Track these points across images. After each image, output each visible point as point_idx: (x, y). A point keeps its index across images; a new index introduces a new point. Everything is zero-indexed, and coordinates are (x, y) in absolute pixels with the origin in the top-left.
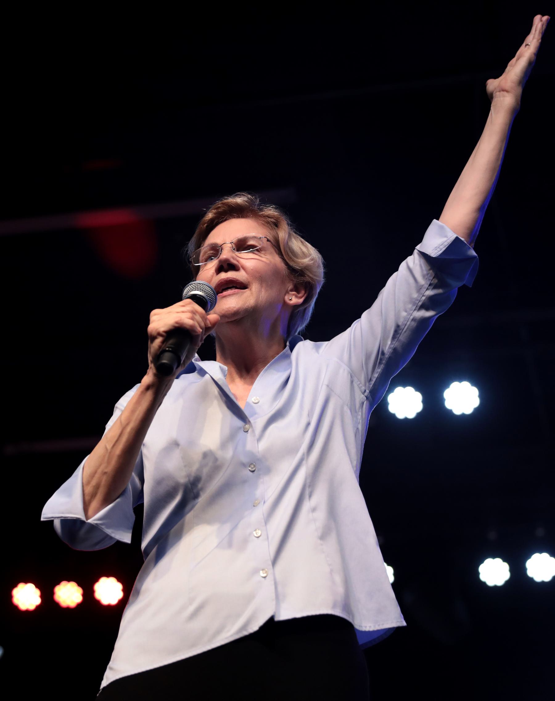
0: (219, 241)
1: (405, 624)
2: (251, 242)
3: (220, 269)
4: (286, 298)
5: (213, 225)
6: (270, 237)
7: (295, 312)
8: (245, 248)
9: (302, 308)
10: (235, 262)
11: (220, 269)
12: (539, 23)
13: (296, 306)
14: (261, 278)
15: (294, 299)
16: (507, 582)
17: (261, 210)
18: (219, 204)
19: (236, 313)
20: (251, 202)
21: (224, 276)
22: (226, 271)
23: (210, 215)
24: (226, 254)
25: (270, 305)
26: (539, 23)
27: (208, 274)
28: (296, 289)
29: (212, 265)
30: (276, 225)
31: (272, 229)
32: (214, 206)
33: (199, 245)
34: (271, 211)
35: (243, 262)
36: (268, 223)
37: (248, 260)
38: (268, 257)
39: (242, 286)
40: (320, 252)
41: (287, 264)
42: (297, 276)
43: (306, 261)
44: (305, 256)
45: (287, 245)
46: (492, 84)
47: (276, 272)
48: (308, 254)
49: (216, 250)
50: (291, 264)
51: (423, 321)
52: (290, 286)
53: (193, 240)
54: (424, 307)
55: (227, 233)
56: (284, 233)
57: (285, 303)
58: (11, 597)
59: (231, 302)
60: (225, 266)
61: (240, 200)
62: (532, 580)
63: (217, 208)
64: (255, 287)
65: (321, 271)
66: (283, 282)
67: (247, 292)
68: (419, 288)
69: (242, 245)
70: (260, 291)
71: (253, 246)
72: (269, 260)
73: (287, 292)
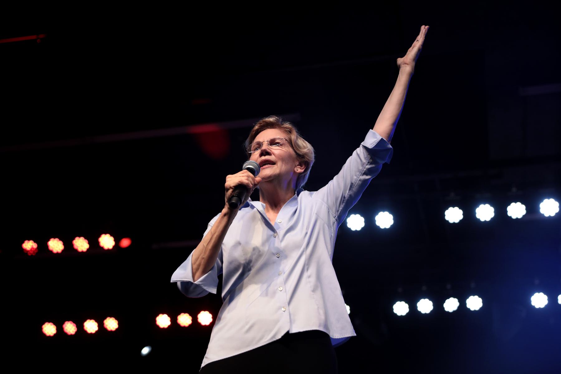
0: (261, 140)
1: (355, 335)
2: (277, 141)
3: (262, 155)
4: (295, 169)
5: (258, 132)
6: (287, 138)
7: (300, 176)
8: (275, 144)
9: (303, 175)
10: (269, 151)
11: (262, 155)
12: (424, 29)
13: (300, 173)
14: (283, 159)
15: (299, 170)
16: (407, 314)
17: (283, 124)
18: (261, 121)
19: (270, 177)
20: (277, 120)
21: (263, 158)
22: (265, 156)
23: (256, 127)
24: (265, 147)
25: (287, 173)
26: (424, 29)
27: (255, 157)
28: (300, 165)
29: (258, 152)
30: (290, 132)
31: (288, 134)
32: (258, 123)
33: (251, 142)
34: (287, 125)
35: (273, 151)
36: (286, 131)
37: (276, 150)
38: (286, 148)
39: (273, 163)
40: (313, 146)
41: (296, 152)
42: (301, 158)
43: (305, 150)
44: (305, 148)
45: (296, 142)
46: (400, 61)
47: (290, 156)
48: (306, 147)
49: (260, 145)
50: (298, 152)
51: (365, 181)
52: (297, 163)
53: (248, 140)
54: (365, 173)
55: (265, 136)
56: (294, 136)
57: (294, 172)
58: (119, 324)
59: (267, 171)
60: (264, 153)
61: (272, 119)
62: (210, 313)
63: (343, 202)
64: (279, 164)
65: (313, 155)
66: (294, 161)
67: (275, 166)
68: (363, 164)
69: (273, 142)
70: (282, 166)
71: (278, 143)
72: (286, 150)
73: (296, 166)
